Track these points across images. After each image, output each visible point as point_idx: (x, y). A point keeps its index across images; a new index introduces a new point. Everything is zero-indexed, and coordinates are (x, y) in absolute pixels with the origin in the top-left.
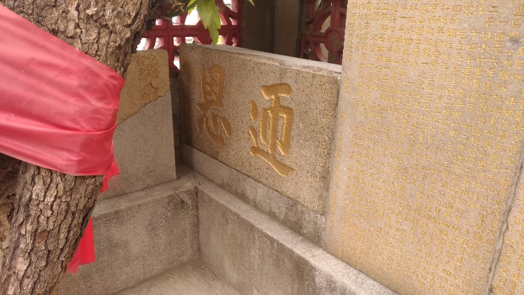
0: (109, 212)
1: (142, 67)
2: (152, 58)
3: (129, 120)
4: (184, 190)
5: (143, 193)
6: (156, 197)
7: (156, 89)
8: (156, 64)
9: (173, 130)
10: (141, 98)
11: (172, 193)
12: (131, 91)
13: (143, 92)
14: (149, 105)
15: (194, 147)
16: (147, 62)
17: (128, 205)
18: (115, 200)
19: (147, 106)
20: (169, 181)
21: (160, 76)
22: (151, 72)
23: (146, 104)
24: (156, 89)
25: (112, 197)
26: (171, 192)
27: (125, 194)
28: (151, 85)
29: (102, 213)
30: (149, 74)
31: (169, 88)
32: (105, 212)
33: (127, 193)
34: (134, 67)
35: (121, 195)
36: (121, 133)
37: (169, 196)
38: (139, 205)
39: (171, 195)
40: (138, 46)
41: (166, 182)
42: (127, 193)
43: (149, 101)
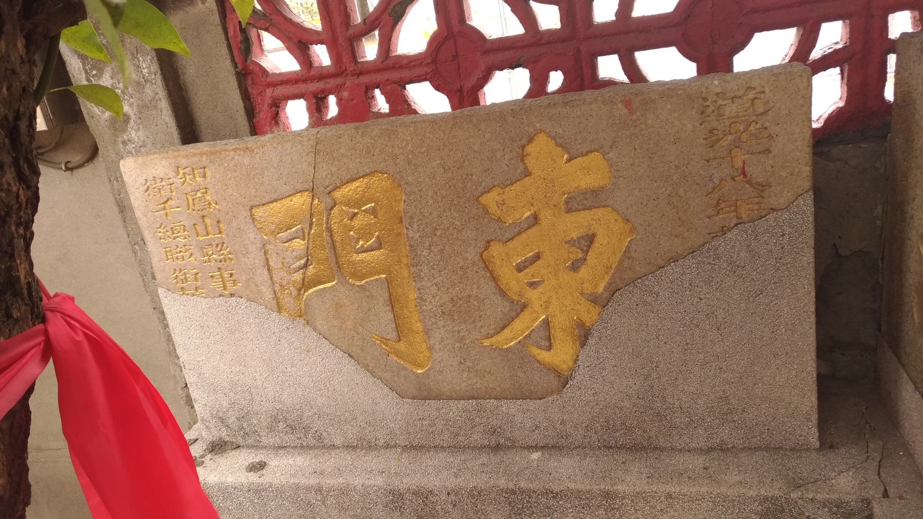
0: (588, 487)
1: (715, 124)
2: (751, 95)
3: (674, 270)
4: (820, 497)
5: (699, 462)
6: (723, 490)
7: (761, 188)
8: (765, 113)
9: (812, 308)
10: (711, 212)
11: (777, 493)
12: (681, 192)
13: (716, 196)
14: (735, 231)
15: (903, 366)
16: (731, 109)
17: (642, 486)
18: (624, 456)
19: (729, 235)
20: (792, 449)
21: (775, 150)
22: (744, 137)
23: (724, 230)
24: (761, 188)
25: (622, 447)
26: (775, 490)
27: (656, 448)
28: (745, 175)
29: (572, 486)
30: (738, 143)
31: (807, 184)
32: (580, 487)
33: (662, 449)
34: (690, 126)
35: (644, 448)
36: (649, 299)
37: (766, 499)
38: (669, 496)
39: (774, 499)
40: (427, 85)
41: (780, 448)
42: (662, 449)
43: (735, 221)
